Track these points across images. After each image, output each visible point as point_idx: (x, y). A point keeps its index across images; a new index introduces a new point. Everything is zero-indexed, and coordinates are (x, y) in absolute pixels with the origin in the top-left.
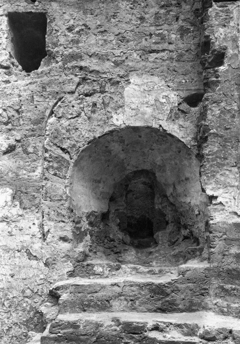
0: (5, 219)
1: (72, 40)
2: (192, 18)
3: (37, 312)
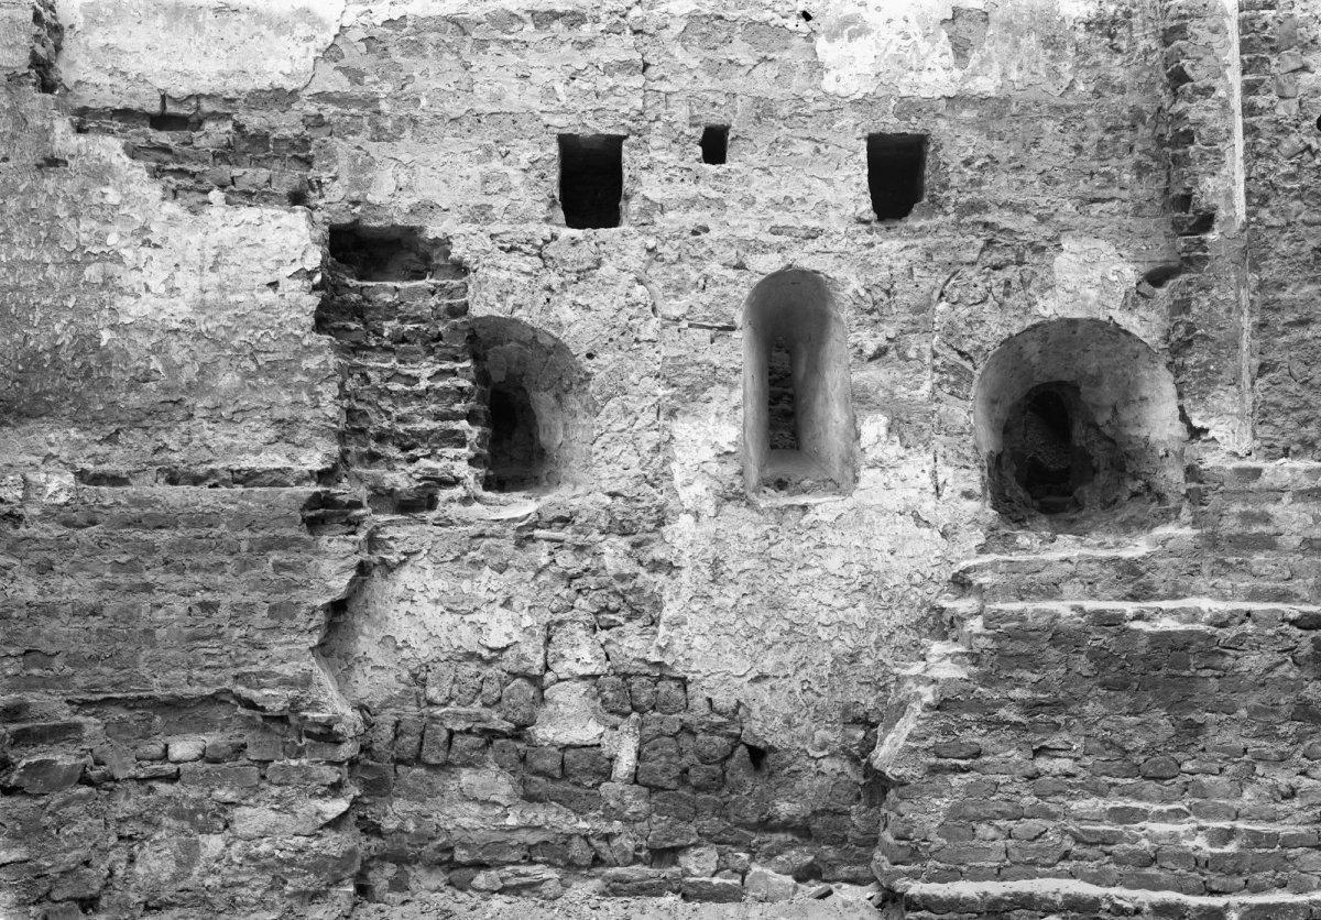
1: (971, 181)
2: (1153, 149)
3: (934, 609)
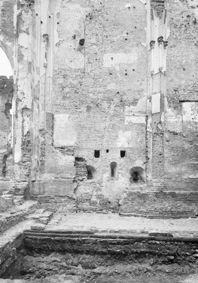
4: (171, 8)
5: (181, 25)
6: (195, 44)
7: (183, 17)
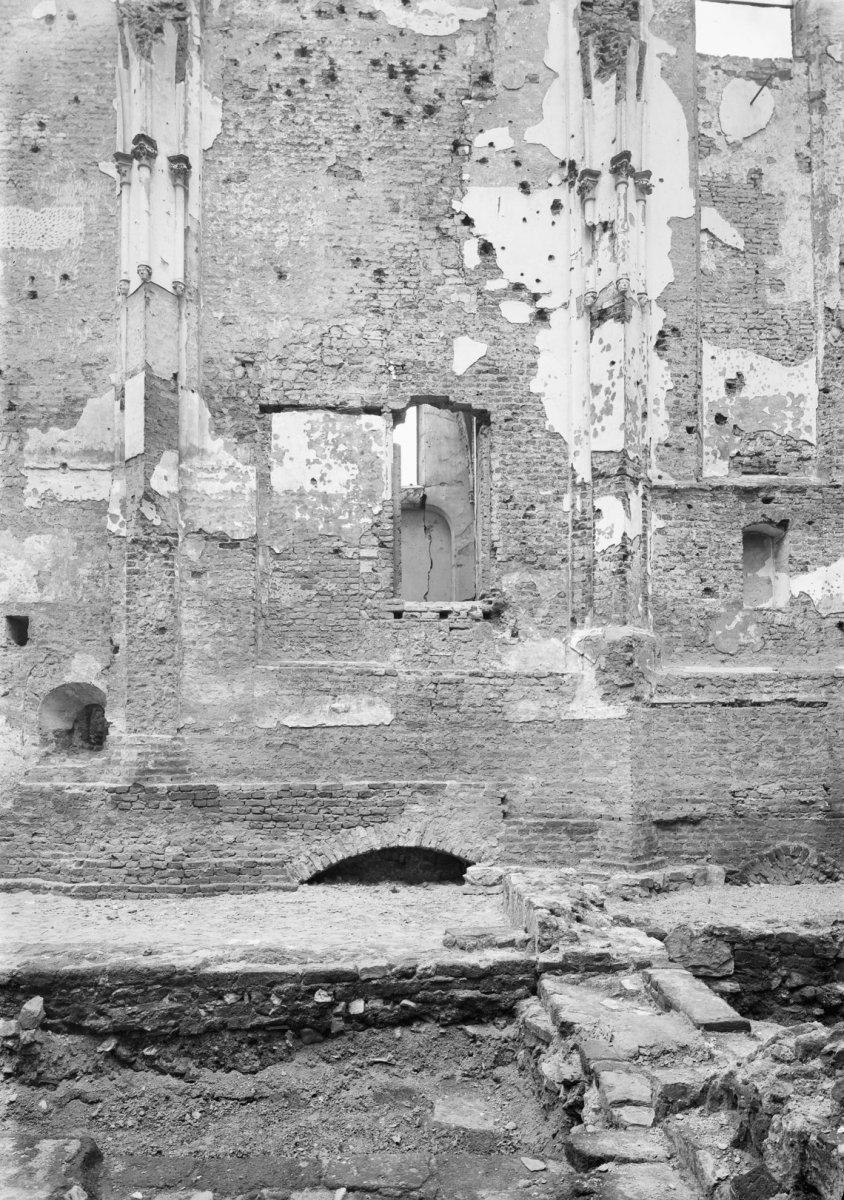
0: (2, 733)
4: (227, 19)
5: (271, 90)
6: (329, 170)
7: (278, 56)
